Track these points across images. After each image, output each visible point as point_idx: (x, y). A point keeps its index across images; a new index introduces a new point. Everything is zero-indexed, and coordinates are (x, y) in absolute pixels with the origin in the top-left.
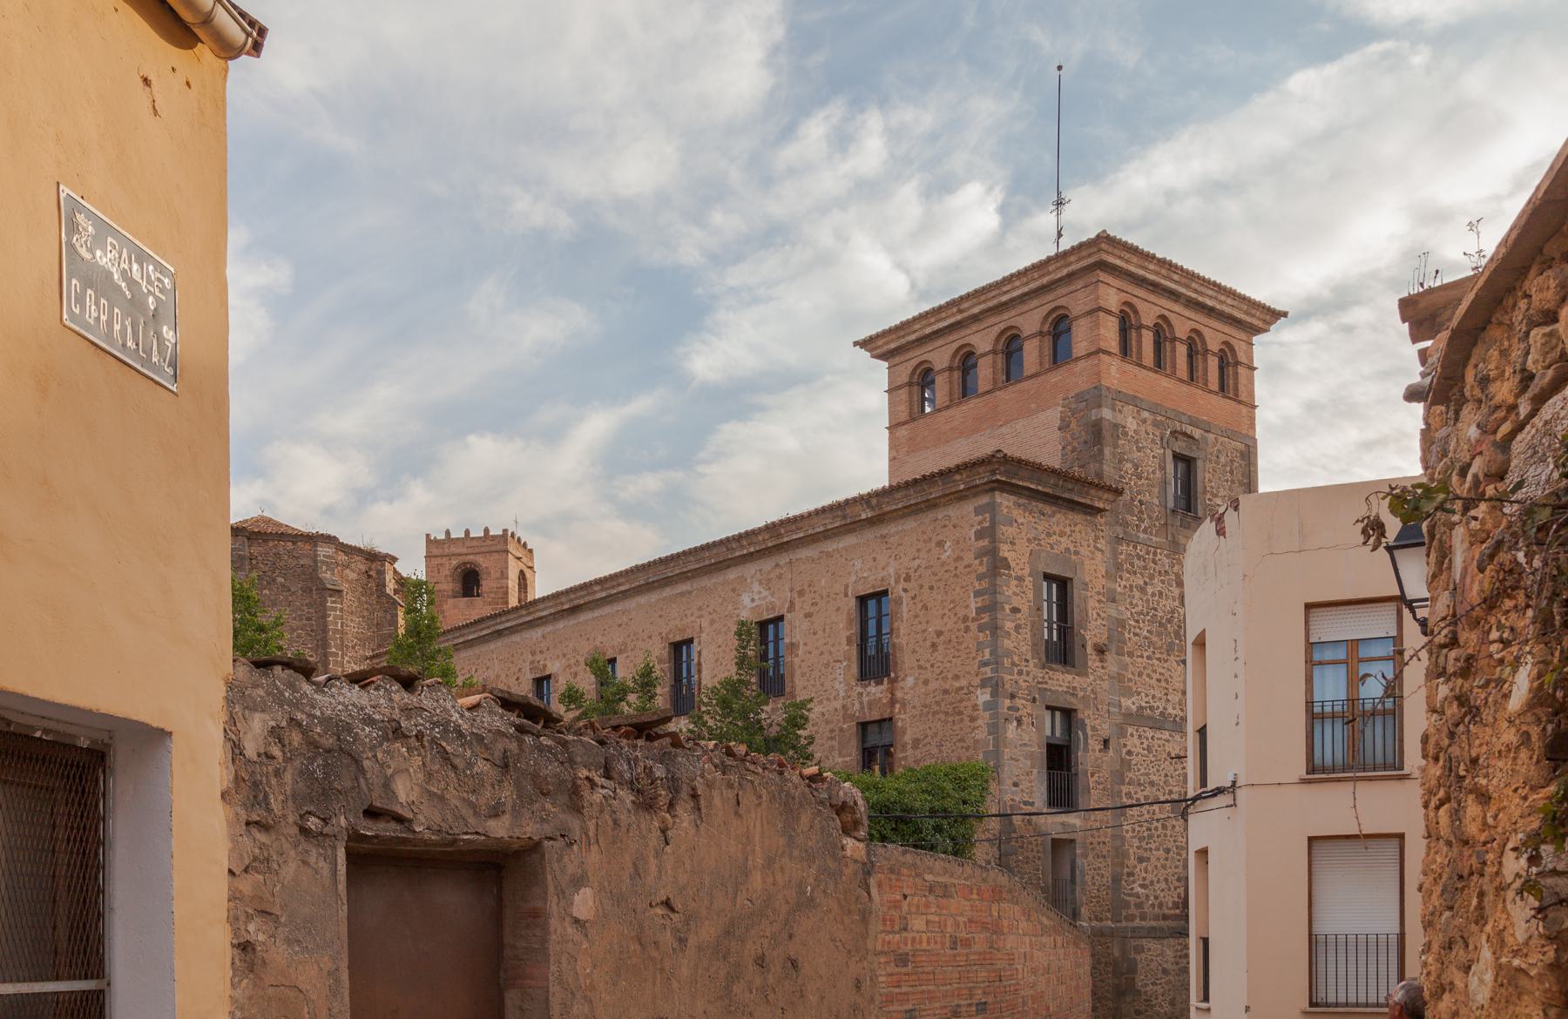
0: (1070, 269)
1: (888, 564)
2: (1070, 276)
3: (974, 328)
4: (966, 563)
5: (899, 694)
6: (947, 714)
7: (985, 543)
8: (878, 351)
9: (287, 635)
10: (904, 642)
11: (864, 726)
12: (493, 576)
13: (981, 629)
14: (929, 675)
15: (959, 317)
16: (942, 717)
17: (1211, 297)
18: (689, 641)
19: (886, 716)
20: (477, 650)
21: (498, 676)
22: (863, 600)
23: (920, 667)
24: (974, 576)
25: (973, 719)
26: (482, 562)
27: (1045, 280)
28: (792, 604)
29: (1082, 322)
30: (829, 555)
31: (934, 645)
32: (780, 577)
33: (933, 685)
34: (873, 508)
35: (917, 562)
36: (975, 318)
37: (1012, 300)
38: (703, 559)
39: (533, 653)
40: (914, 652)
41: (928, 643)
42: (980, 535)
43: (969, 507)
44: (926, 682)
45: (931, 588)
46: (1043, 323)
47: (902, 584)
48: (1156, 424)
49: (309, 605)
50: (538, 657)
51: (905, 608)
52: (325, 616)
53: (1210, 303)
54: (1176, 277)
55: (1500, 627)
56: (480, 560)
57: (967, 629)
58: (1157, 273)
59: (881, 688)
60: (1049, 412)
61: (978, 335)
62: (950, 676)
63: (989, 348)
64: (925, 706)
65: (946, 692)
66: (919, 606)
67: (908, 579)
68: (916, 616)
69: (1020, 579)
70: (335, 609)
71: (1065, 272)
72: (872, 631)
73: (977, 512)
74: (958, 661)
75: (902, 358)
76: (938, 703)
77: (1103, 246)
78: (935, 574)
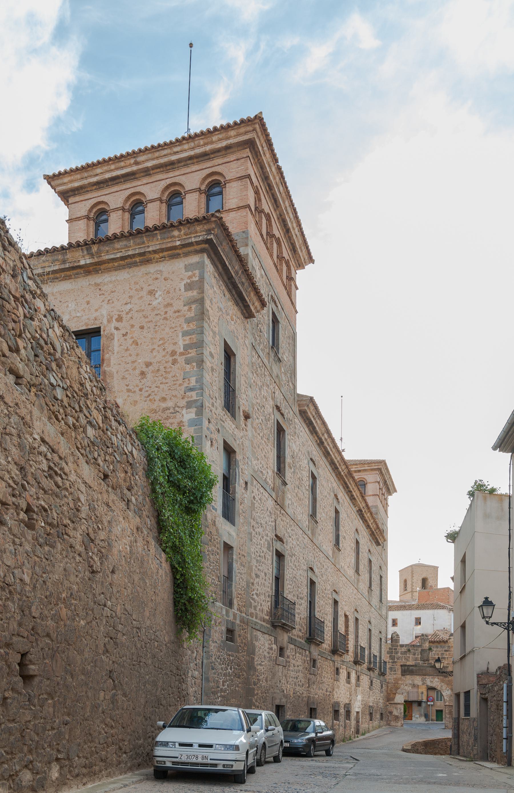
1: (100, 307)
2: (228, 148)
3: (145, 180)
4: (175, 308)
7: (194, 294)
10: (114, 370)
13: (188, 362)
14: (137, 398)
15: (135, 168)
23: (129, 391)
24: (182, 320)
27: (208, 148)
29: (234, 184)
31: (143, 373)
34: (92, 256)
35: (129, 307)
36: (147, 172)
37: (179, 161)
40: (124, 378)
41: (138, 372)
42: (189, 287)
43: (178, 265)
45: (142, 328)
46: (202, 183)
47: (114, 324)
51: (116, 342)
55: (50, 613)
57: (175, 362)
62: (157, 398)
67: (120, 319)
68: (127, 350)
71: (224, 144)
73: (187, 268)
74: (165, 387)
75: (82, 198)
78: (145, 317)
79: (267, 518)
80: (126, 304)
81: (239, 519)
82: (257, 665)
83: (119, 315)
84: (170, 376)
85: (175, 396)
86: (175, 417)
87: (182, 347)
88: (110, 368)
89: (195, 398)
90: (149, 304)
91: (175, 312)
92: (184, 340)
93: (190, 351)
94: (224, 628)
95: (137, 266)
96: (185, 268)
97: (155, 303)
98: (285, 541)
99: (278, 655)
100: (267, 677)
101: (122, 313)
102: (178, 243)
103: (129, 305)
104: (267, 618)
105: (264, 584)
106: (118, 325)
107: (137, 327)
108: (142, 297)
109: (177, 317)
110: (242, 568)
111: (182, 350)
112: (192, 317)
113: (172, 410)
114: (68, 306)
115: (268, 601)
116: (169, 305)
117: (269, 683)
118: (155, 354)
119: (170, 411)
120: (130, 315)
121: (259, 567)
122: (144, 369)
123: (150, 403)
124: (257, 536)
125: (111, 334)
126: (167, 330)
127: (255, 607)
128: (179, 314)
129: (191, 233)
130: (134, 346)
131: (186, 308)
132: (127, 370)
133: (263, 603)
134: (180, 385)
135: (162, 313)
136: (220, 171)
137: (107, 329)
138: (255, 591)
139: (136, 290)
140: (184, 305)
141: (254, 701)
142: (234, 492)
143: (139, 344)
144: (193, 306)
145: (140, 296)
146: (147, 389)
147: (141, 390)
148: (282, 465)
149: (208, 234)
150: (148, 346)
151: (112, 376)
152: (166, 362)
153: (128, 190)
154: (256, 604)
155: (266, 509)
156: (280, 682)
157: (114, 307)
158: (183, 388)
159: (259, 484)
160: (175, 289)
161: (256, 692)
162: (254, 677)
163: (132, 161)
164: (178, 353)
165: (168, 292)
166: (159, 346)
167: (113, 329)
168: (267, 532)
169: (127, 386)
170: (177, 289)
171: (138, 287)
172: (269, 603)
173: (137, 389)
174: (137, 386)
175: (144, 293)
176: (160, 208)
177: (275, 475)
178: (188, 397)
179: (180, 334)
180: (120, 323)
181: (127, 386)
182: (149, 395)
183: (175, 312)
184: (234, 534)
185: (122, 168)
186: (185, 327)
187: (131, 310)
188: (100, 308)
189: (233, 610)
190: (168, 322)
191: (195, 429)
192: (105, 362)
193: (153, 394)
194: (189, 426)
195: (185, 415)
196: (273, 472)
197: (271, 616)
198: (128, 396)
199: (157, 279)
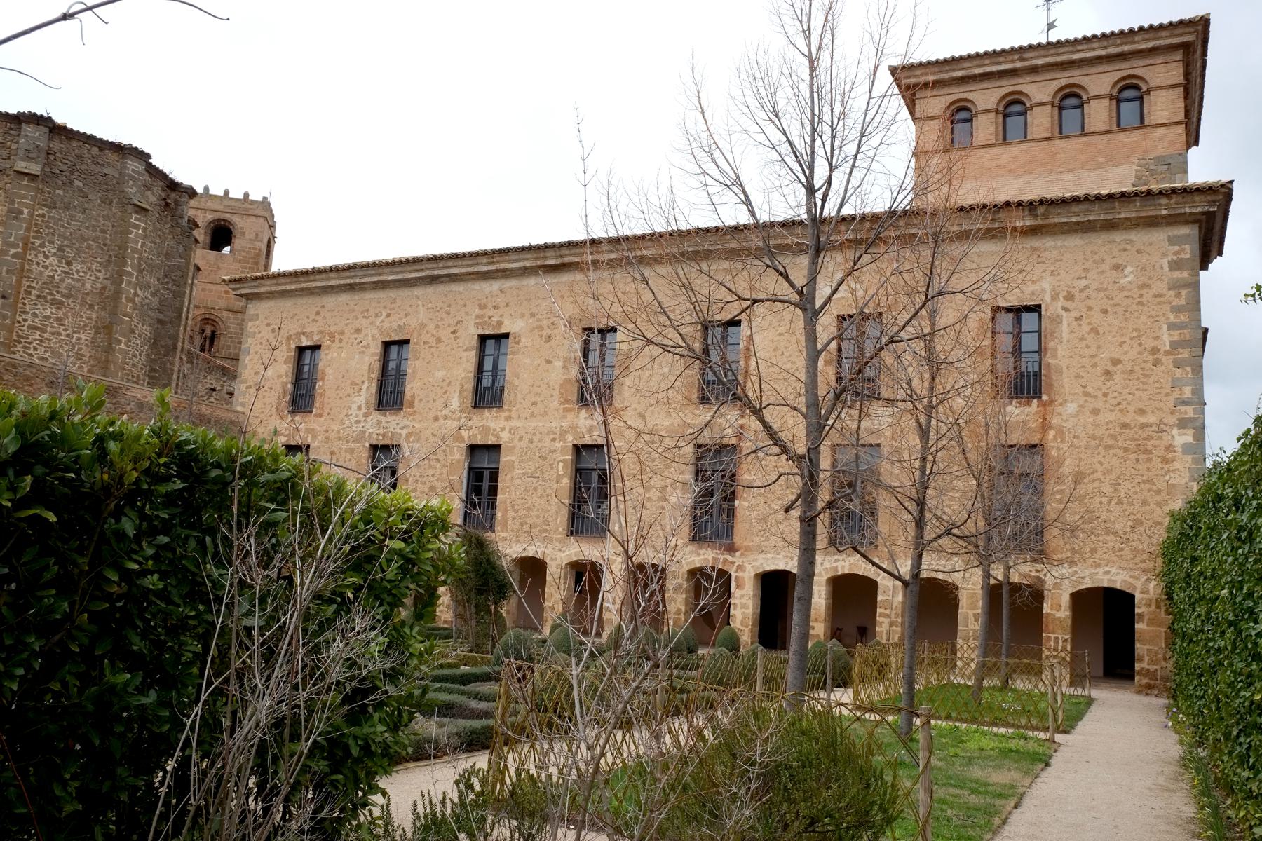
0: (1157, 43)
5: (1055, 421)
6: (1126, 450)
9: (1116, 323)
10: (1063, 363)
11: (578, 449)
12: (247, 236)
14: (1099, 404)
15: (1018, 65)
16: (1120, 453)
18: (316, 348)
19: (1035, 441)
20: (393, 293)
21: (423, 326)
22: (387, 345)
23: (1086, 394)
24: (1167, 308)
25: (1166, 461)
26: (238, 222)
27: (1126, 48)
33: (1105, 416)
35: (1083, 283)
36: (1034, 70)
38: (545, 258)
39: (483, 307)
40: (1078, 376)
41: (1099, 370)
43: (1159, 236)
47: (1062, 302)
49: (107, 218)
50: (489, 312)
52: (126, 233)
56: (235, 219)
57: (1156, 363)
59: (1028, 409)
60: (1121, 168)
63: (992, 105)
68: (1082, 339)
70: (137, 227)
71: (1150, 44)
72: (488, 365)
74: (1145, 395)
76: (1113, 437)
80: (1079, 278)
84: (1151, 380)
85: (1160, 409)
86: (1160, 438)
87: (1168, 344)
91: (1155, 296)
97: (1123, 281)
102: (1164, 212)
106: (1067, 304)
107: (1097, 310)
108: (1103, 272)
109: (1159, 303)
111: (1168, 347)
116: (1144, 286)
120: (1085, 294)
122: (1110, 367)
126: (1144, 318)
130: (1093, 335)
131: (1172, 293)
134: (1167, 395)
144: (1184, 292)
158: (1171, 400)
163: (1016, 57)
171: (1096, 257)
173: (1100, 394)
174: (1100, 389)
179: (1165, 327)
182: (1119, 403)
183: (1155, 296)
185: (1001, 63)
187: (1086, 287)
190: (1145, 309)
195: (1177, 437)
199: (1125, 250)
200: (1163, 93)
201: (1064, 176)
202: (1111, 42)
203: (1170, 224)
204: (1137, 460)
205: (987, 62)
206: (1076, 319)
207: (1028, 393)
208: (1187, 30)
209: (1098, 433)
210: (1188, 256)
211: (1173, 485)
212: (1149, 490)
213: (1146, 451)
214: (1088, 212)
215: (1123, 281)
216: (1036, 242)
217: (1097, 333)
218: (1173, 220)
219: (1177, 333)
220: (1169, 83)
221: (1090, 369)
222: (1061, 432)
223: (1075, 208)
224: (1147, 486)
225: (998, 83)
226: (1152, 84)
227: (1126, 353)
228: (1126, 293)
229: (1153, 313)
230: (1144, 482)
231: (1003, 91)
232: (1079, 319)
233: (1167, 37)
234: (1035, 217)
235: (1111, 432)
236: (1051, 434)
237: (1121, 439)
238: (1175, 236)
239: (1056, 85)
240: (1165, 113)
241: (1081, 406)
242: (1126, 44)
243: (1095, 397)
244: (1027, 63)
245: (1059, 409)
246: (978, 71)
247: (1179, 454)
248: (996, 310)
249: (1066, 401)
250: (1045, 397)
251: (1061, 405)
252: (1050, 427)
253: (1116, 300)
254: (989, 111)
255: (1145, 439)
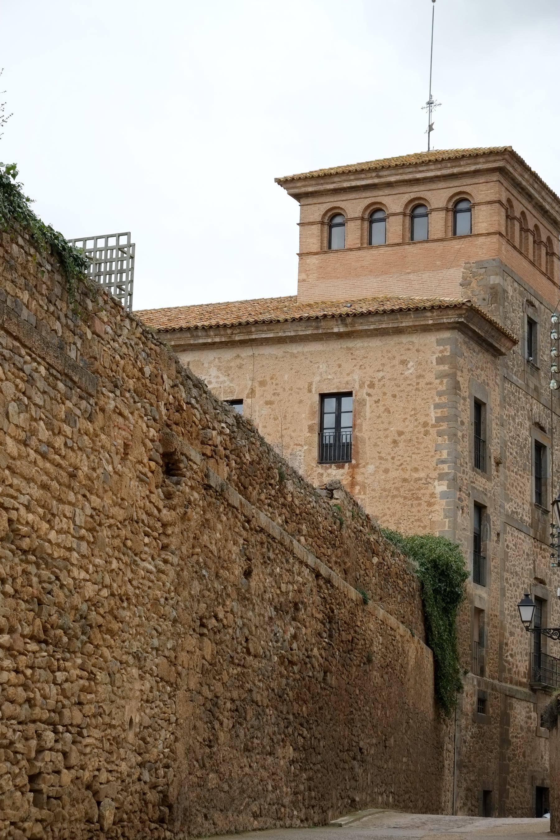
1: (352, 372)
5: (359, 478)
6: (405, 498)
8: (296, 191)
9: (401, 404)
10: (367, 437)
13: (440, 434)
14: (389, 465)
15: (376, 181)
16: (401, 500)
17: (549, 203)
23: (381, 458)
24: (434, 392)
25: (430, 504)
27: (456, 170)
28: (252, 392)
30: (293, 356)
31: (395, 442)
32: (240, 367)
33: (393, 474)
35: (381, 374)
36: (389, 185)
40: (376, 445)
41: (389, 440)
43: (431, 339)
44: (386, 471)
47: (366, 390)
48: (521, 294)
51: (368, 409)
53: (548, 207)
54: (536, 186)
57: (426, 433)
58: (527, 181)
59: (341, 471)
60: (452, 270)
61: (390, 198)
62: (409, 468)
64: (384, 490)
65: (405, 480)
66: (382, 409)
68: (379, 417)
69: (464, 399)
71: (473, 168)
74: (418, 457)
76: (397, 489)
77: (507, 157)
79: (524, 563)
80: (378, 371)
81: (492, 578)
82: (513, 737)
83: (371, 382)
84: (422, 447)
85: (427, 467)
86: (427, 488)
87: (434, 419)
88: (362, 434)
89: (446, 470)
90: (402, 374)
91: (427, 384)
92: (436, 413)
93: (442, 424)
94: (475, 699)
95: (390, 335)
96: (437, 342)
97: (407, 373)
98: (547, 581)
99: (539, 725)
100: (524, 752)
101: (374, 380)
102: (431, 322)
103: (381, 372)
104: (525, 680)
105: (520, 641)
106: (370, 391)
107: (389, 394)
108: (394, 366)
109: (429, 389)
110: (495, 629)
111: (434, 422)
112: (444, 391)
113: (424, 481)
114: (318, 367)
115: (525, 661)
116: (420, 376)
117: (527, 758)
118: (407, 424)
119: (422, 482)
120: (382, 383)
121: (514, 624)
122: (397, 438)
123: (402, 472)
124: (511, 588)
125: (363, 400)
126: (419, 400)
127: (510, 670)
128: (431, 386)
129: (443, 315)
130: (386, 414)
131: (438, 381)
132: (379, 438)
133: (519, 664)
134: (432, 456)
135: (415, 384)
136: (468, 191)
137: (359, 394)
138: (510, 652)
139: (389, 358)
140: (436, 379)
141: (509, 779)
142: (485, 550)
143: (391, 412)
144: (445, 381)
145: (392, 364)
146: (399, 457)
147: (393, 458)
148: (543, 488)
149: (459, 317)
150: (400, 415)
151: (364, 442)
152: (419, 433)
153: (368, 199)
154: (511, 666)
155: (522, 552)
156: (542, 757)
157: (366, 373)
158: (435, 460)
159: (513, 529)
160: (427, 361)
161: (511, 769)
162: (509, 751)
163: (374, 174)
164: (430, 425)
165: (420, 364)
166: (411, 416)
167: (365, 395)
168: (523, 579)
169: (379, 453)
170: (429, 361)
171: (390, 355)
172: (527, 663)
173: (389, 457)
174: (389, 454)
175: (396, 362)
176: (403, 222)
177: (534, 507)
178: (440, 470)
179: (432, 406)
180: (372, 389)
181: (379, 453)
182: (402, 464)
183: (427, 384)
184: (485, 595)
186: (437, 400)
187: (383, 377)
188: (351, 373)
189: (485, 678)
190: (420, 393)
191: (446, 502)
192: (357, 427)
193: (405, 463)
194: (441, 498)
195: (437, 487)
196: (531, 504)
197: (529, 678)
198: (381, 463)
199: (409, 349)
200: (484, 208)
201: (411, 276)
202: (443, 165)
203: (438, 330)
204: (412, 505)
205: (352, 177)
206: (376, 402)
207: (343, 459)
208: (497, 158)
209: (388, 487)
210: (448, 354)
211: (434, 522)
212: (419, 526)
213: (418, 498)
214: (381, 322)
215: (407, 373)
216: (350, 344)
217: (389, 412)
218: (438, 327)
219: (439, 411)
220: (488, 199)
221: (383, 439)
222: (364, 487)
223: (372, 319)
224: (418, 523)
225: (364, 195)
226: (477, 200)
227: (407, 426)
228: (408, 382)
229: (425, 397)
230: (416, 521)
231: (368, 202)
232: (377, 402)
233: (484, 163)
234: (346, 325)
235: (396, 485)
236: (357, 488)
237: (402, 490)
238: (441, 339)
239: (406, 198)
240: (484, 225)
241: (377, 467)
242: (455, 167)
243: (386, 460)
244: (383, 180)
245: (362, 470)
246: (346, 185)
247: (438, 499)
248: (323, 396)
249: (367, 464)
250: (354, 462)
251: (364, 467)
252: (357, 484)
253: (402, 388)
254: (355, 219)
255: (418, 489)
